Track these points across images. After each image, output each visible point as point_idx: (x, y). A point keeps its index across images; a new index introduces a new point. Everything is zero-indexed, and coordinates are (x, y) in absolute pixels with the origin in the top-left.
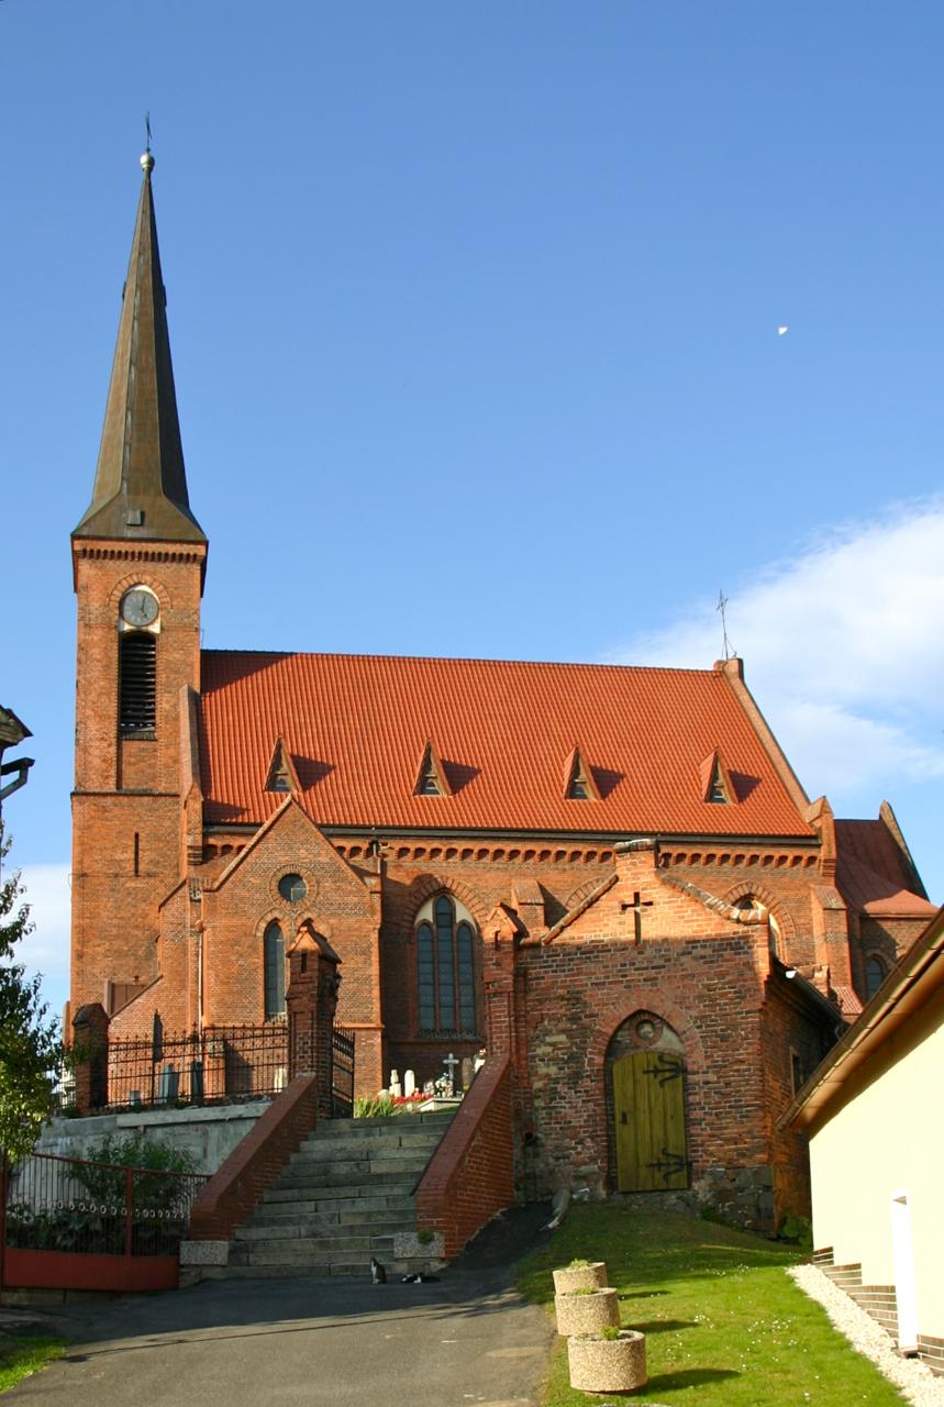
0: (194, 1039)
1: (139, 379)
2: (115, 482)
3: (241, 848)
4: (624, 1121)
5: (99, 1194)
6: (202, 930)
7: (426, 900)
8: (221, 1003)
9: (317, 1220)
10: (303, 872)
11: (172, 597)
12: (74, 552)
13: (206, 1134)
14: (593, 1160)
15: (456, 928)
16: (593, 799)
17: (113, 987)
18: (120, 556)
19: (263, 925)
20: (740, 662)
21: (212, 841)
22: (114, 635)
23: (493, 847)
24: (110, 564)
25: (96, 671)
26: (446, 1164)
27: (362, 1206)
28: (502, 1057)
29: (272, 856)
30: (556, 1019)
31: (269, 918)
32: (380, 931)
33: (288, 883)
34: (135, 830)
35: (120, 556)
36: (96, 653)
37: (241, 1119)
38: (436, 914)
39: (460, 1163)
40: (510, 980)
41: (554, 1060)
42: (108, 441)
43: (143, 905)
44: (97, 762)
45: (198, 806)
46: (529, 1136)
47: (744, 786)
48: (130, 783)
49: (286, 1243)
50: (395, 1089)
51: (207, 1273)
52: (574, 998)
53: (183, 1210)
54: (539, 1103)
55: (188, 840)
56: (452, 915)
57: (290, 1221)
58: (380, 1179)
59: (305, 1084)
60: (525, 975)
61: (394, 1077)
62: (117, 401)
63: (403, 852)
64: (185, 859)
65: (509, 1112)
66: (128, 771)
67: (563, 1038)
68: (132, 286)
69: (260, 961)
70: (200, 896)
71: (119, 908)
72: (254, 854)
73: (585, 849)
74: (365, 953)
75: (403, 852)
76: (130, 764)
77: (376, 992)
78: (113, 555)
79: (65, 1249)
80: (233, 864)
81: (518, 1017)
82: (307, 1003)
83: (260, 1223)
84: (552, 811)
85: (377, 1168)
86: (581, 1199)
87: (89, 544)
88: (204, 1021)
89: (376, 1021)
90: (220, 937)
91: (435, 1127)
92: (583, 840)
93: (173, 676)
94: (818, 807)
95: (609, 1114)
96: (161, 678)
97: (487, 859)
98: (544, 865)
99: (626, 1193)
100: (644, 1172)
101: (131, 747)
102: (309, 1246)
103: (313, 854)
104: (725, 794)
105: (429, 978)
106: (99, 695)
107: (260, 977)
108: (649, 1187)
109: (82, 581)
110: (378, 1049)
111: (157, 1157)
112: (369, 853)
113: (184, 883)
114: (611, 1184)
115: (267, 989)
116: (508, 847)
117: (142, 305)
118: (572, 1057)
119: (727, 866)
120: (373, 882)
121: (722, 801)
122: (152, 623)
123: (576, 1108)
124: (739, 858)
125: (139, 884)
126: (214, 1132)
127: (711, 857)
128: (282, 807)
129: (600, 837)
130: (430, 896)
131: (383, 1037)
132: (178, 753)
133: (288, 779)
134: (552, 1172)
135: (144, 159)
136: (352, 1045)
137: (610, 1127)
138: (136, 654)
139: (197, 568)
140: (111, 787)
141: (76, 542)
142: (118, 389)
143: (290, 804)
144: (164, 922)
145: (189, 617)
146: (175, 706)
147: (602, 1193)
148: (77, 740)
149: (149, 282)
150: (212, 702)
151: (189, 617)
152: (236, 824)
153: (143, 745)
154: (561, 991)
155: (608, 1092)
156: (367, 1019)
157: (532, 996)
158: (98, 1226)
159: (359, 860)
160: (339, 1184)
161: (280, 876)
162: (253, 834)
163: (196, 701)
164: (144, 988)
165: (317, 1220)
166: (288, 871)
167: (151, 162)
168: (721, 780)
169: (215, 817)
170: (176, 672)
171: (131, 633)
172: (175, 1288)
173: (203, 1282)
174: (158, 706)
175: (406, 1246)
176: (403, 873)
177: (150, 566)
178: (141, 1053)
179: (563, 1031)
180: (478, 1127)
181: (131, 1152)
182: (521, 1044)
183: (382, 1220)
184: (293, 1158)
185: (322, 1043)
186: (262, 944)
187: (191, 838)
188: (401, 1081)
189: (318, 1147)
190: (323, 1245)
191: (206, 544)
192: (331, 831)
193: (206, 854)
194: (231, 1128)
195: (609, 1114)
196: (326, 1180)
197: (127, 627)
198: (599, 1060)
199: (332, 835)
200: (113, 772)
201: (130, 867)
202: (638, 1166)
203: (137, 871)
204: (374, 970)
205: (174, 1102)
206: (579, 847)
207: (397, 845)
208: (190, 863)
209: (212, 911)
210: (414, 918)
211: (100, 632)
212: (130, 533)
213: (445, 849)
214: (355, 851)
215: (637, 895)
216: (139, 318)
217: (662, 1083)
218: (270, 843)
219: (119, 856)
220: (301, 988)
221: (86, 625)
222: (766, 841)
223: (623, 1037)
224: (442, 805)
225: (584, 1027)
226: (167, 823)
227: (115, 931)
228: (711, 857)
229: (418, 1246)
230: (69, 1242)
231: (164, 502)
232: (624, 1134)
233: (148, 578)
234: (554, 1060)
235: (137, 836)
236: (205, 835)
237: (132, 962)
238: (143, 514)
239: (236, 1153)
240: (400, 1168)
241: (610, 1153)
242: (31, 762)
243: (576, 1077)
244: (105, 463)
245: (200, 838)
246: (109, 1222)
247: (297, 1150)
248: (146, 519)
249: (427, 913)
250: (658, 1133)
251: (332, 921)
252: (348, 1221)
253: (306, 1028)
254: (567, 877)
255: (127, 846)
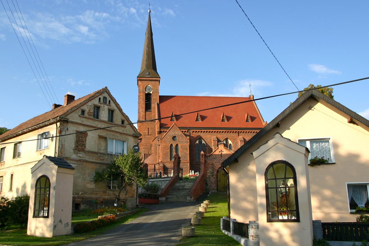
0: (158, 163)
1: (148, 50)
2: (144, 67)
3: (166, 131)
4: (219, 181)
5: (147, 190)
6: (160, 145)
7: (197, 140)
8: (163, 158)
9: (177, 195)
10: (176, 136)
11: (154, 87)
12: (138, 80)
13: (162, 182)
14: (215, 187)
15: (202, 144)
16: (226, 122)
17: (144, 154)
18: (145, 80)
19: (170, 145)
20: (253, 96)
21: (161, 130)
22: (144, 94)
23: (208, 131)
24: (144, 82)
25: (141, 100)
26: (194, 187)
27: (183, 193)
28: (202, 174)
29: (171, 133)
30: (210, 167)
31: (171, 143)
32: (189, 146)
33: (174, 138)
34: (148, 127)
35: (145, 80)
36: (141, 97)
37: (167, 180)
38: (199, 142)
39: (196, 187)
40: (204, 162)
41: (210, 173)
42: (143, 60)
43: (149, 140)
44: (142, 116)
45: (159, 124)
46: (206, 183)
47: (253, 119)
48: (147, 119)
49: (173, 198)
50: (191, 173)
51: (163, 202)
52: (213, 164)
53: (159, 193)
54: (208, 179)
55: (157, 130)
56: (202, 142)
57: (173, 195)
58: (186, 189)
59: (176, 175)
60: (206, 161)
61: (191, 171)
62: (145, 53)
63: (193, 132)
64: (157, 133)
65: (203, 179)
66: (147, 117)
67: (211, 170)
68: (147, 33)
69: (169, 151)
70: (159, 139)
71: (145, 141)
72: (168, 133)
73: (224, 131)
74: (187, 149)
75: (193, 132)
76: (147, 116)
77: (189, 156)
78: (144, 80)
79: (143, 198)
80: (165, 135)
81: (205, 167)
82: (176, 164)
83: (169, 195)
84: (219, 124)
85: (185, 188)
86: (213, 192)
87: (140, 78)
88: (160, 161)
89: (189, 161)
90: (163, 147)
91: (193, 182)
92: (224, 129)
93: (154, 101)
94: (265, 123)
95: (217, 180)
96: (152, 101)
97: (208, 133)
98: (217, 134)
99: (219, 191)
100: (222, 188)
101: (147, 113)
102: (176, 198)
103: (178, 133)
104: (249, 120)
105: (198, 153)
106: (142, 104)
107: (169, 153)
108: (222, 191)
109: (139, 85)
110: (189, 166)
111: (155, 186)
112: (188, 132)
113: (157, 137)
114: (217, 190)
115: (170, 156)
116: (211, 131)
117: (149, 36)
118: (212, 172)
119: (249, 133)
120: (188, 137)
121: (249, 122)
122: (151, 92)
123: (213, 180)
124: (251, 132)
125: (149, 136)
126: (163, 182)
127: (246, 132)
128: (173, 125)
129: (227, 129)
130: (198, 139)
131: (190, 163)
132: (155, 114)
133: (174, 119)
134: (209, 189)
135: (149, 11)
136: (182, 170)
137: (217, 182)
138: (148, 97)
139: (158, 82)
140: (144, 120)
141: (138, 78)
142: (145, 51)
143: (174, 124)
144: (153, 143)
145: (157, 90)
146: (155, 106)
147: (216, 191)
148: (138, 112)
149: (150, 32)
150: (161, 105)
151: (157, 90)
152: (164, 127)
153: (149, 113)
154: (211, 163)
155: (217, 177)
156: (187, 160)
157: (207, 164)
158: (147, 195)
159: (186, 133)
160: (180, 190)
161: (172, 136)
162: (168, 129)
163: (158, 105)
164: (150, 155)
165: (177, 195)
166: (174, 136)
167: (150, 11)
168: (249, 118)
169: (162, 126)
170: (155, 100)
171: (147, 93)
172: (158, 204)
173: (162, 203)
174: (152, 106)
175: (188, 198)
176: (194, 135)
177: (150, 82)
178: (153, 171)
179: (211, 169)
180: (199, 182)
181: (152, 185)
182: (205, 171)
183: (186, 195)
184: (174, 186)
185: (178, 168)
186: (169, 148)
187: (158, 130)
188: (192, 172)
189: (177, 185)
190: (178, 198)
191: (160, 78)
192: (181, 128)
193: (160, 132)
194: (165, 182)
195: (217, 180)
196: (178, 189)
197: (147, 92)
198: (216, 173)
199: (181, 129)
200: (144, 117)
201: (147, 133)
202: (221, 188)
203: (148, 134)
204: (188, 152)
205: (157, 178)
206: (223, 131)
207: (192, 130)
208: (157, 134)
209: (161, 142)
210: (195, 143)
211: (142, 93)
212: (147, 76)
213: (200, 131)
214: (185, 132)
215: (221, 150)
216: (148, 38)
217: (224, 176)
218: (171, 131)
219: (145, 132)
220: (175, 162)
221: (140, 92)
222: (256, 129)
223: (219, 170)
224: (200, 123)
225: (214, 168)
226: (153, 126)
227: (145, 144)
228: (246, 132)
229: (190, 198)
230: (144, 197)
231: (153, 70)
232: (219, 183)
233: (150, 84)
234: (210, 173)
235: (148, 128)
236: (160, 129)
237: (147, 150)
238: (149, 73)
239: (166, 185)
240: (188, 188)
241: (217, 186)
242: (142, 139)
243: (213, 175)
244: (142, 64)
245: (159, 130)
246: (149, 195)
247: (175, 185)
248: (150, 73)
249: (197, 142)
250: (224, 184)
251: (181, 144)
252: (181, 195)
253: (176, 168)
254: (221, 136)
255: (147, 130)
